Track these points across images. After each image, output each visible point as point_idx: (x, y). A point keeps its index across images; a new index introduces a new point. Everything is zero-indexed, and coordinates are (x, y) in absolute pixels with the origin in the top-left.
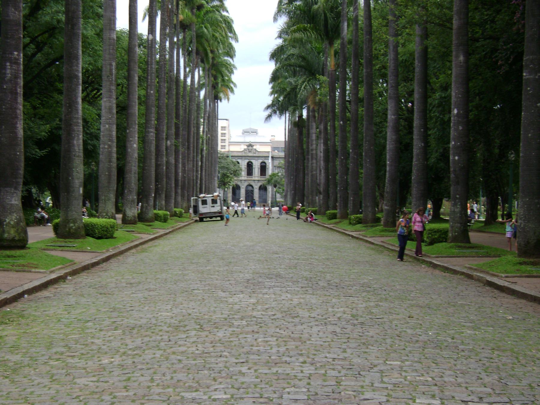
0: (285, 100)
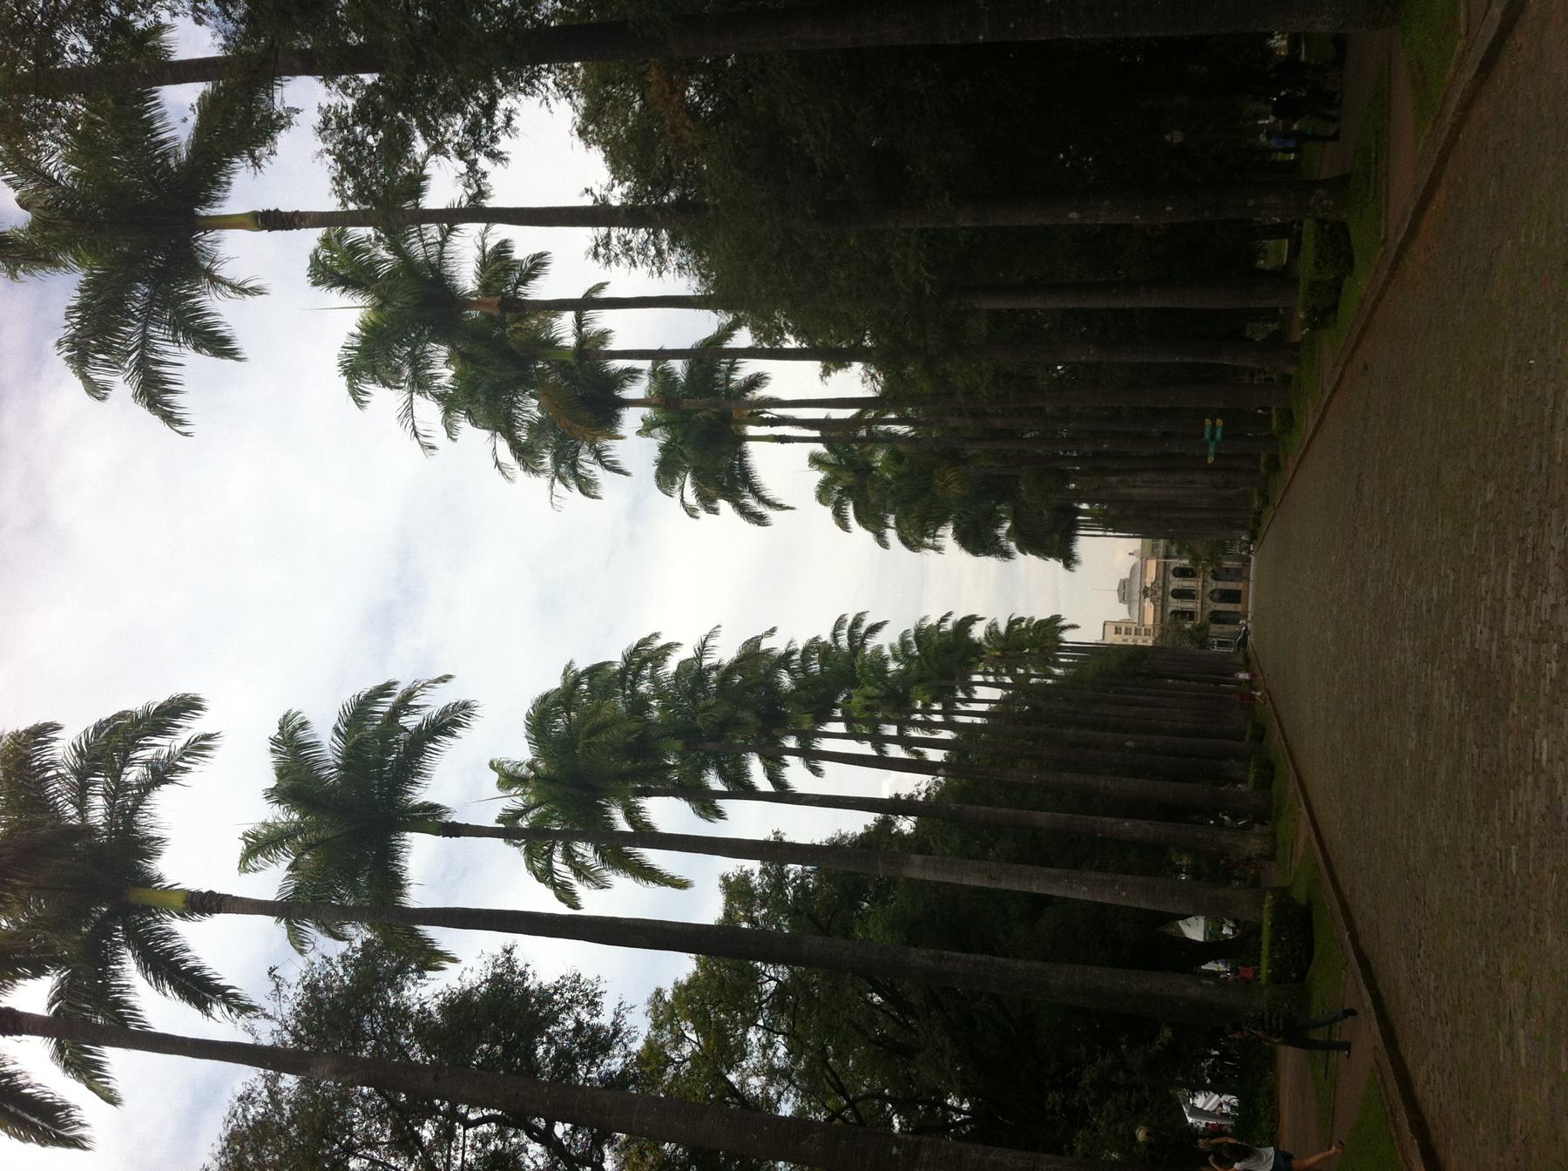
0: (1054, 542)
